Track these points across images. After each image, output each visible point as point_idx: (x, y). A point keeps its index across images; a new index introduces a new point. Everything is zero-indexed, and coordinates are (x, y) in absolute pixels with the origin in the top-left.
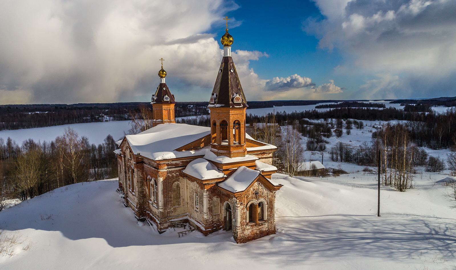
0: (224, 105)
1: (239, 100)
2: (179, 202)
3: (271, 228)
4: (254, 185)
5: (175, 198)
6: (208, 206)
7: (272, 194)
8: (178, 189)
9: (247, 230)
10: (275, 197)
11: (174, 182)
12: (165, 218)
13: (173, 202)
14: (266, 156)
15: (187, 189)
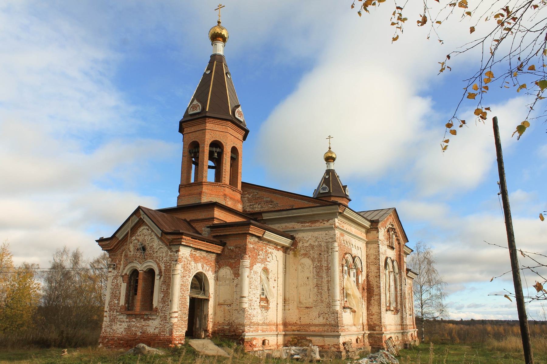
1: (196, 108)
3: (163, 331)
4: (138, 233)
7: (172, 254)
9: (120, 323)
10: (176, 261)
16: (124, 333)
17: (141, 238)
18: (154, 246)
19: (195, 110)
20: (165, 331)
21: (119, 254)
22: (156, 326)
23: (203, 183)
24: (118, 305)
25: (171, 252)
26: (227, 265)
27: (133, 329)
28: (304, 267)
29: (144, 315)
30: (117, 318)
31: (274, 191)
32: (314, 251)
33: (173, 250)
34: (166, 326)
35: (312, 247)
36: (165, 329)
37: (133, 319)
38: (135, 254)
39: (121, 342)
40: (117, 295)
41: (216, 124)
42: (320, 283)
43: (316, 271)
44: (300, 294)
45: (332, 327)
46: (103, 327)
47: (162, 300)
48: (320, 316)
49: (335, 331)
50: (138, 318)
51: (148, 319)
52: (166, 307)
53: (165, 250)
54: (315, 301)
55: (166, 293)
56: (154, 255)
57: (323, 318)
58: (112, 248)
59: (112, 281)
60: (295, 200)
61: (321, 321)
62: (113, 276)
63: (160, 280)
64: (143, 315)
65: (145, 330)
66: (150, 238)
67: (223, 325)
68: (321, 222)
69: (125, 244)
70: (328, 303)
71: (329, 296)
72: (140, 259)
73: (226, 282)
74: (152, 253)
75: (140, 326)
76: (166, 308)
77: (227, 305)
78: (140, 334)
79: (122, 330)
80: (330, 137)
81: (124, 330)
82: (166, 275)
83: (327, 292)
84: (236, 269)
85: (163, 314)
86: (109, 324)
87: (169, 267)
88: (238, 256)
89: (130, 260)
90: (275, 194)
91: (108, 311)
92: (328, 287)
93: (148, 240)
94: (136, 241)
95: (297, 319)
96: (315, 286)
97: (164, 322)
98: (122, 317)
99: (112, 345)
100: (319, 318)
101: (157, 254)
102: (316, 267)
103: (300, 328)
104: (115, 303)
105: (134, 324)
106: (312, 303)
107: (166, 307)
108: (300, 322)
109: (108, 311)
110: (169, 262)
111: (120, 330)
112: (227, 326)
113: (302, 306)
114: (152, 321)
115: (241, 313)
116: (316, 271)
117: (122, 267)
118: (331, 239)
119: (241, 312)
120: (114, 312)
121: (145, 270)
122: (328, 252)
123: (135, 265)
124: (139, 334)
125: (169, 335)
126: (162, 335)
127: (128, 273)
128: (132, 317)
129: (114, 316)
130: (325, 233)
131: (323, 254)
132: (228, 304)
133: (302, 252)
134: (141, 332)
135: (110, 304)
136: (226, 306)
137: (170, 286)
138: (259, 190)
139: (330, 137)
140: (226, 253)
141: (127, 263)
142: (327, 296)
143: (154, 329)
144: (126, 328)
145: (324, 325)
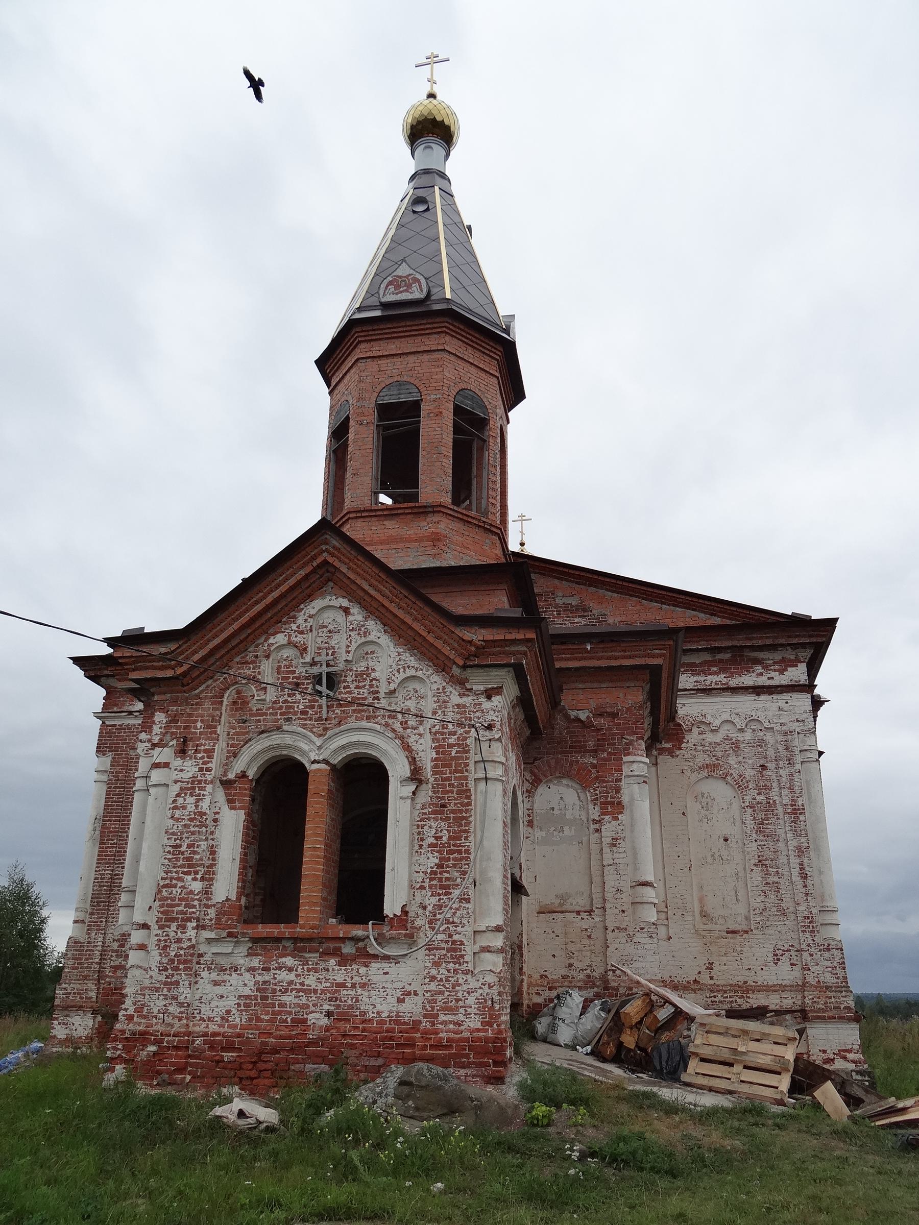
1: (409, 286)
3: (447, 1009)
4: (300, 621)
7: (467, 700)
9: (214, 976)
14: (763, 681)
15: (516, 903)
16: (238, 1019)
17: (312, 641)
18: (374, 670)
22: (408, 988)
24: (205, 901)
26: (567, 775)
27: (288, 999)
28: (710, 804)
29: (343, 940)
30: (201, 955)
32: (741, 758)
33: (475, 687)
34: (459, 985)
35: (736, 746)
36: (457, 1000)
37: (285, 956)
38: (286, 701)
39: (228, 1056)
40: (201, 859)
41: (471, 343)
42: (768, 854)
47: (431, 879)
48: (778, 960)
49: (842, 1006)
50: (307, 955)
51: (365, 956)
52: (457, 909)
53: (435, 687)
55: (451, 852)
57: (792, 964)
58: (179, 671)
59: (174, 801)
60: (664, 606)
61: (785, 973)
62: (176, 782)
63: (413, 800)
64: (340, 938)
65: (350, 1002)
66: (357, 640)
67: (566, 984)
68: (761, 675)
69: (237, 659)
70: (805, 917)
71: (807, 895)
72: (311, 719)
74: (365, 698)
75: (320, 987)
76: (454, 913)
77: (578, 913)
78: (325, 1021)
79: (231, 1002)
80: (524, 518)
81: (239, 1005)
82: (444, 780)
84: (606, 787)
88: (614, 744)
89: (259, 721)
90: (595, 587)
91: (152, 922)
92: (801, 869)
93: (348, 646)
94: (287, 653)
95: (699, 969)
96: (755, 865)
97: (449, 971)
98: (227, 948)
99: (181, 1070)
100: (776, 964)
101: (393, 700)
102: (754, 807)
103: (715, 997)
104: (191, 892)
105: (292, 977)
108: (712, 978)
109: (152, 922)
110: (454, 733)
111: (213, 1004)
112: (586, 988)
114: (387, 965)
117: (221, 748)
118: (798, 724)
120: (184, 927)
121: (336, 762)
122: (790, 762)
123: (288, 739)
124: (318, 1019)
125: (479, 1025)
126: (444, 1023)
127: (251, 774)
128: (278, 948)
129: (185, 945)
130: (775, 706)
132: (578, 909)
133: (702, 759)
134: (329, 1014)
135: (165, 894)
137: (469, 823)
138: (541, 574)
139: (524, 518)
140: (556, 733)
141: (247, 733)
143: (394, 1000)
144: (248, 997)
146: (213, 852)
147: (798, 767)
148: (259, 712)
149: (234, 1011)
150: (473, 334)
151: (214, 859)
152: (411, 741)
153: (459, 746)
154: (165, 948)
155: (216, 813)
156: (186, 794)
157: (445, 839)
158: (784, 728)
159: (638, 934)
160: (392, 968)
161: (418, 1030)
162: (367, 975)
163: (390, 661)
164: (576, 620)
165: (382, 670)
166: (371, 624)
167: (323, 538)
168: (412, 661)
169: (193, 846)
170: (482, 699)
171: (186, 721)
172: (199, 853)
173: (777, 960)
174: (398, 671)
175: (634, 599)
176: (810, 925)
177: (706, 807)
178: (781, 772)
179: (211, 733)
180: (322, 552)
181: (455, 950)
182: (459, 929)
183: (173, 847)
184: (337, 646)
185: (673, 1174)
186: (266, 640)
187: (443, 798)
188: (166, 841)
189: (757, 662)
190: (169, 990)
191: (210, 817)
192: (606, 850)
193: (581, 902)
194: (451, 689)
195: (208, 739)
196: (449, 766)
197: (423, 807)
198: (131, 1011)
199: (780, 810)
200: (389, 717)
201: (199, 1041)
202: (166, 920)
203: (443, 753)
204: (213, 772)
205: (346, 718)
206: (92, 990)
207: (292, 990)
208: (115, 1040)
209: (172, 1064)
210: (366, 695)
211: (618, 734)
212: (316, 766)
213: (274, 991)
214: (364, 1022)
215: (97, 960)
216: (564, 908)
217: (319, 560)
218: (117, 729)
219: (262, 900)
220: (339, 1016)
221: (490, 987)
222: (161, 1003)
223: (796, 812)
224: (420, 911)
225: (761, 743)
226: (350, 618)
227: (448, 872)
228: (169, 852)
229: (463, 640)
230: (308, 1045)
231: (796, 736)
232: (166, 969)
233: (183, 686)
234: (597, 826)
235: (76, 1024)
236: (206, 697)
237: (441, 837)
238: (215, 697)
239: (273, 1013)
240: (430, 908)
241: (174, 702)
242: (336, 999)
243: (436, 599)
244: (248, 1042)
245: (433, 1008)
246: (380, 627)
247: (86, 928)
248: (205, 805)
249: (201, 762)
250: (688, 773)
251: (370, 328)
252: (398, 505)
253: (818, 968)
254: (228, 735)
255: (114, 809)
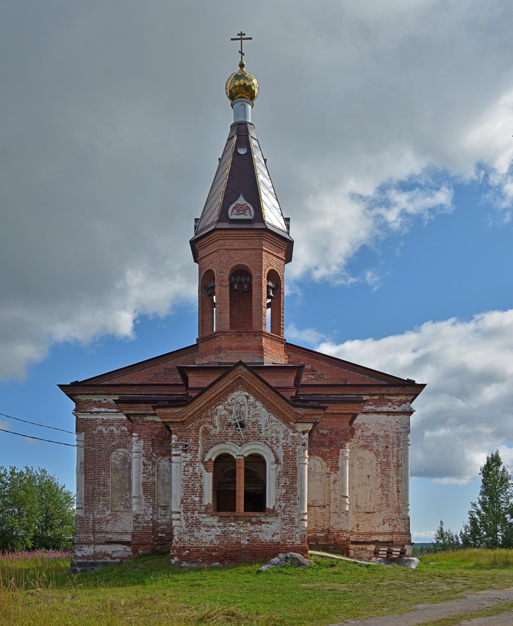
0: (215, 301)
1: (244, 211)
2: (127, 500)
4: (229, 400)
5: (117, 490)
6: (142, 480)
7: (296, 435)
8: (125, 468)
9: (206, 529)
11: (114, 448)
12: (87, 532)
13: (109, 498)
18: (259, 421)
19: (243, 214)
20: (293, 538)
21: (192, 429)
22: (275, 532)
23: (264, 334)
24: (200, 504)
25: (293, 432)
27: (234, 536)
28: (363, 462)
31: (317, 355)
32: (378, 443)
34: (294, 531)
35: (376, 437)
36: (293, 536)
38: (225, 432)
39: (214, 554)
41: (273, 243)
42: (385, 482)
43: (381, 468)
44: (357, 496)
45: (403, 536)
46: (174, 534)
47: (283, 497)
48: (385, 523)
49: (407, 540)
50: (239, 522)
52: (293, 507)
53: (283, 429)
54: (378, 505)
56: (261, 435)
57: (390, 525)
59: (184, 469)
60: (350, 372)
61: (387, 528)
62: (184, 462)
68: (390, 407)
69: (204, 415)
71: (398, 499)
72: (235, 439)
73: (314, 477)
74: (256, 432)
75: (244, 532)
76: (291, 509)
77: (320, 507)
78: (247, 543)
79: (213, 537)
80: (243, 37)
81: (216, 538)
83: (396, 495)
85: (287, 516)
86: (188, 529)
87: (292, 453)
88: (337, 444)
89: (215, 439)
92: (397, 489)
95: (353, 527)
97: (290, 527)
103: (359, 537)
104: (195, 501)
105: (234, 529)
106: (374, 507)
107: (291, 506)
110: (291, 447)
111: (207, 538)
112: (322, 533)
113: (359, 511)
115: (343, 517)
116: (381, 468)
118: (403, 429)
119: (343, 516)
120: (194, 513)
125: (300, 543)
126: (288, 542)
127: (213, 459)
128: (229, 520)
131: (390, 446)
133: (362, 443)
134: (248, 540)
136: (318, 507)
137: (296, 479)
139: (243, 37)
140: (314, 438)
142: (396, 499)
143: (271, 536)
144: (219, 535)
145: (392, 533)
146: (201, 487)
147: (401, 447)
148: (214, 436)
149: (214, 540)
150: (208, 238)
151: (202, 490)
152: (274, 449)
153: (293, 451)
154: (187, 520)
155: (201, 473)
156: (188, 466)
157: (288, 484)
158: (398, 431)
159: (342, 515)
160: (270, 526)
161: (280, 545)
162: (261, 528)
163: (266, 419)
164: (309, 376)
165: (262, 422)
166: (258, 403)
167: (239, 368)
168: (274, 419)
169: (194, 485)
170: (301, 434)
171: (185, 439)
172: (196, 488)
173: (384, 523)
174: (269, 422)
175: (337, 367)
176: (398, 510)
177: (362, 463)
178: (394, 449)
179: (196, 443)
180: (238, 373)
181: (292, 520)
182: (293, 514)
183: (186, 485)
184: (244, 411)
185: (361, 196)
186: (215, 407)
187: (287, 470)
188: (183, 483)
189: (389, 401)
190: (190, 533)
191: (199, 475)
192: (332, 484)
193: (321, 503)
194: (289, 430)
195: (195, 446)
196: (289, 458)
197: (280, 472)
198: (177, 540)
199: (392, 465)
200: (266, 439)
201: (203, 549)
202: (186, 511)
203: (287, 454)
204: (199, 458)
205: (249, 439)
206: (91, 537)
207: (235, 533)
208: (173, 549)
209: (195, 556)
210: (256, 431)
211: (338, 440)
212: (238, 457)
213: (228, 533)
214: (260, 542)
215: (91, 525)
216: (314, 505)
217: (238, 377)
218: (85, 421)
219: (274, 557)
220: (252, 541)
221: (304, 531)
222: (188, 538)
223: (398, 466)
224: (279, 508)
225: (387, 436)
226: (249, 400)
227: (289, 495)
228: (184, 487)
229: (296, 413)
230: (242, 550)
231: (402, 434)
232: (188, 527)
233: (183, 424)
234: (328, 475)
235: (86, 550)
236: (192, 429)
237: (286, 483)
238: (196, 429)
239: (228, 540)
240: (283, 507)
241: (180, 431)
242: (251, 536)
243: (259, 375)
244: (221, 549)
245: (285, 538)
246: (262, 405)
247: (84, 511)
248: (197, 470)
249: (193, 454)
250: (355, 448)
251: (225, 233)
252: (271, 334)
253: (399, 526)
254: (203, 444)
255: (148, 491)
